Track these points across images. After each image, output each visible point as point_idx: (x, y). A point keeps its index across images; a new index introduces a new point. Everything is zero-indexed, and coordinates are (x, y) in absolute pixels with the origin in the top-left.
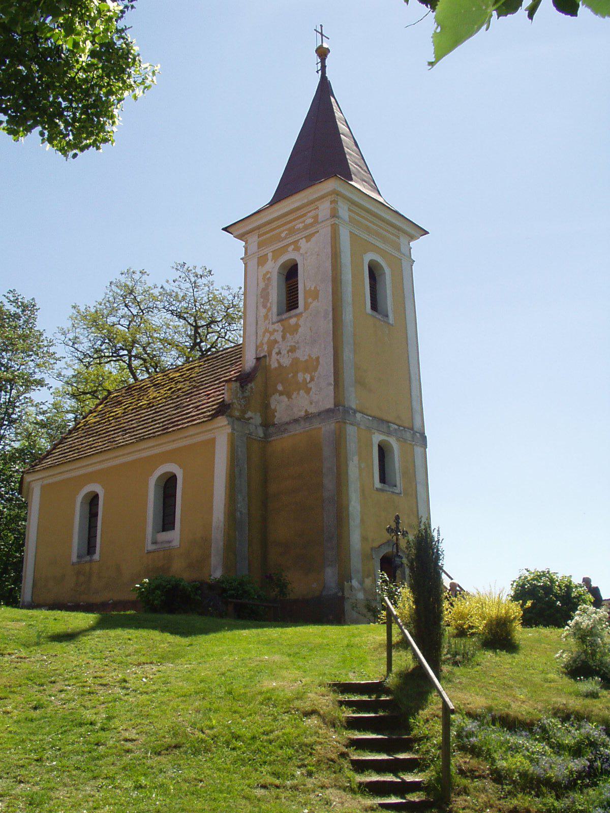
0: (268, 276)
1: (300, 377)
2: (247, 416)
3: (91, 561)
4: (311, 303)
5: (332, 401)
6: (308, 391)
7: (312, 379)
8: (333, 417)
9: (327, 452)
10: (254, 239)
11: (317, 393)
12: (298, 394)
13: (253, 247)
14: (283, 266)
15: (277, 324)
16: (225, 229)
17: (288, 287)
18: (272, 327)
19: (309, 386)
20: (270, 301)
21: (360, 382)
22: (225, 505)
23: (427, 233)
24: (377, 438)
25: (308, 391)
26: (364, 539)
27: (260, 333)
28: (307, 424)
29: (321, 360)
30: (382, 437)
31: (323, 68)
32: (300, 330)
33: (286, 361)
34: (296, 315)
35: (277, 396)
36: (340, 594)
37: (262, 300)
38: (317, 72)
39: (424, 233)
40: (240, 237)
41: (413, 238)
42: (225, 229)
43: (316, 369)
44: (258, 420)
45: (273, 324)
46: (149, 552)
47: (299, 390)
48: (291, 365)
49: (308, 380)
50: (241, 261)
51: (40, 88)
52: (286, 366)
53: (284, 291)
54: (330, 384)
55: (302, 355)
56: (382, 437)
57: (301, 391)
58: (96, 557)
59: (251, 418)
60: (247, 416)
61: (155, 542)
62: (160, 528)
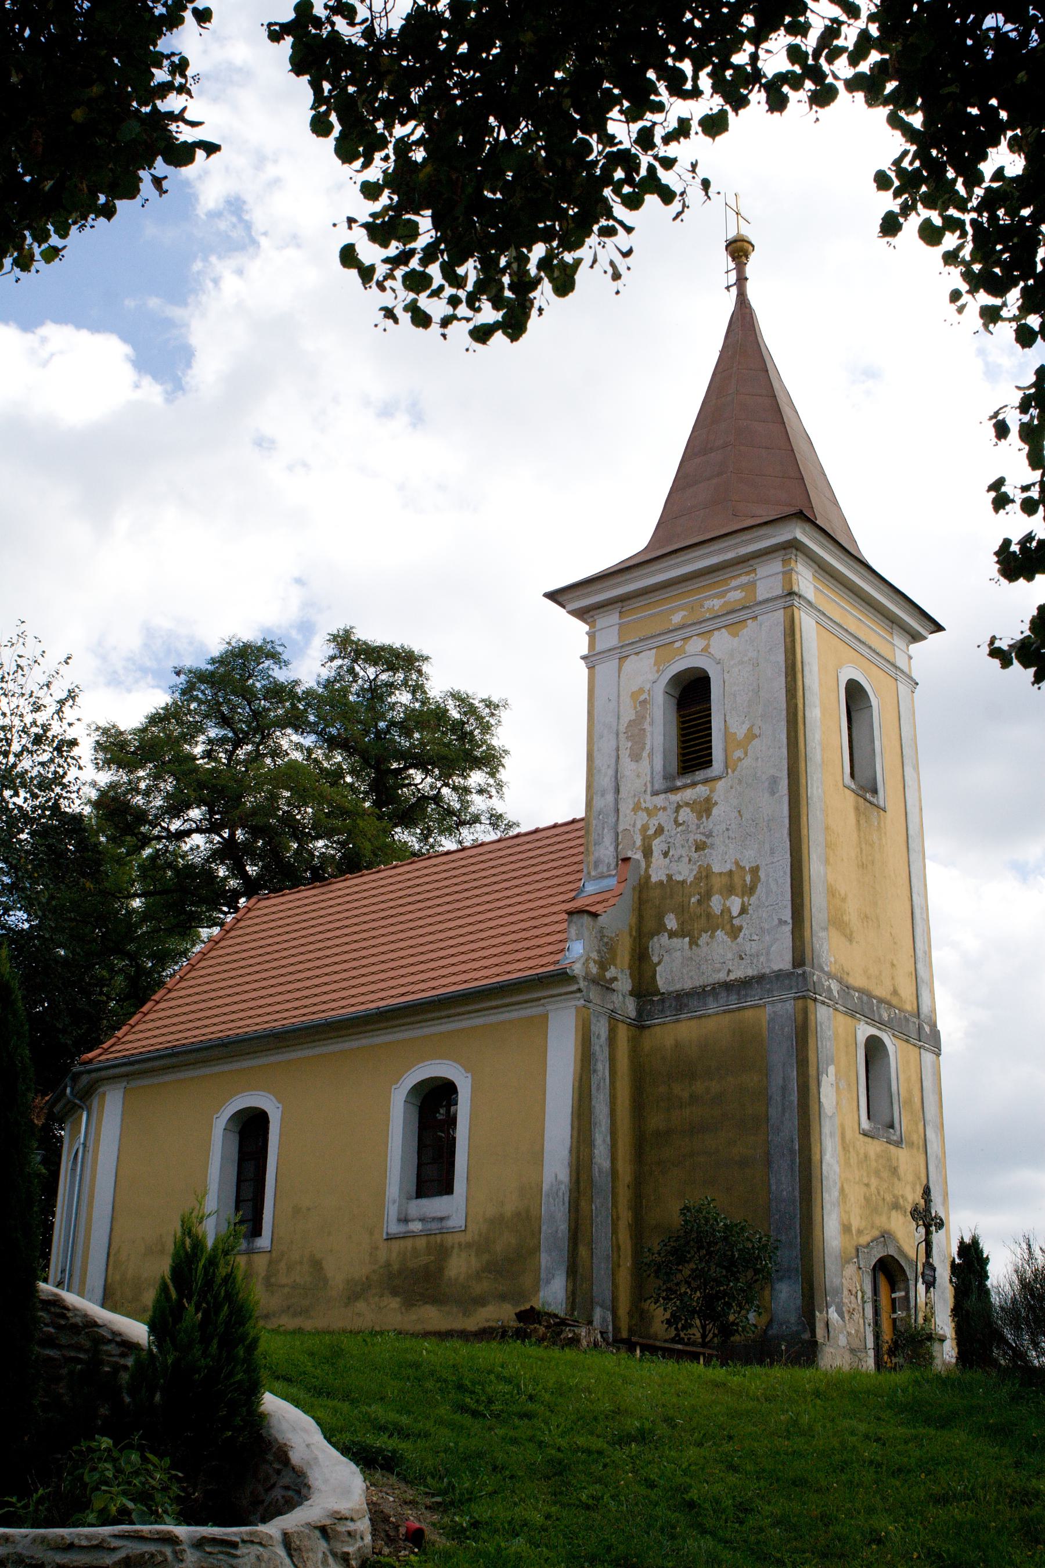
0: (642, 698)
1: (716, 903)
2: (608, 975)
3: (250, 1252)
4: (740, 759)
5: (788, 957)
6: (735, 932)
7: (743, 911)
8: (791, 988)
9: (780, 1055)
10: (611, 620)
11: (755, 937)
12: (712, 937)
13: (609, 639)
14: (676, 679)
15: (663, 796)
16: (553, 596)
17: (683, 723)
18: (649, 801)
19: (736, 922)
20: (648, 747)
21: (838, 923)
22: (571, 1151)
23: (939, 628)
24: (865, 1031)
25: (735, 932)
26: (846, 1229)
27: (626, 808)
28: (733, 998)
29: (762, 874)
30: (873, 1031)
31: (741, 281)
32: (715, 811)
33: (684, 872)
34: (706, 781)
35: (664, 939)
36: (806, 1336)
37: (629, 744)
38: (728, 288)
39: (933, 627)
40: (581, 614)
41: (916, 637)
42: (553, 596)
43: (751, 890)
44: (624, 984)
45: (655, 793)
46: (390, 1238)
47: (714, 931)
48: (698, 878)
49: (735, 911)
50: (582, 662)
51: (999, 247)
52: (684, 882)
53: (674, 731)
54: (782, 922)
55: (720, 863)
56: (873, 1031)
57: (719, 932)
58: (264, 1242)
59: (615, 979)
60: (608, 975)
61: (404, 1220)
62: (412, 1188)
